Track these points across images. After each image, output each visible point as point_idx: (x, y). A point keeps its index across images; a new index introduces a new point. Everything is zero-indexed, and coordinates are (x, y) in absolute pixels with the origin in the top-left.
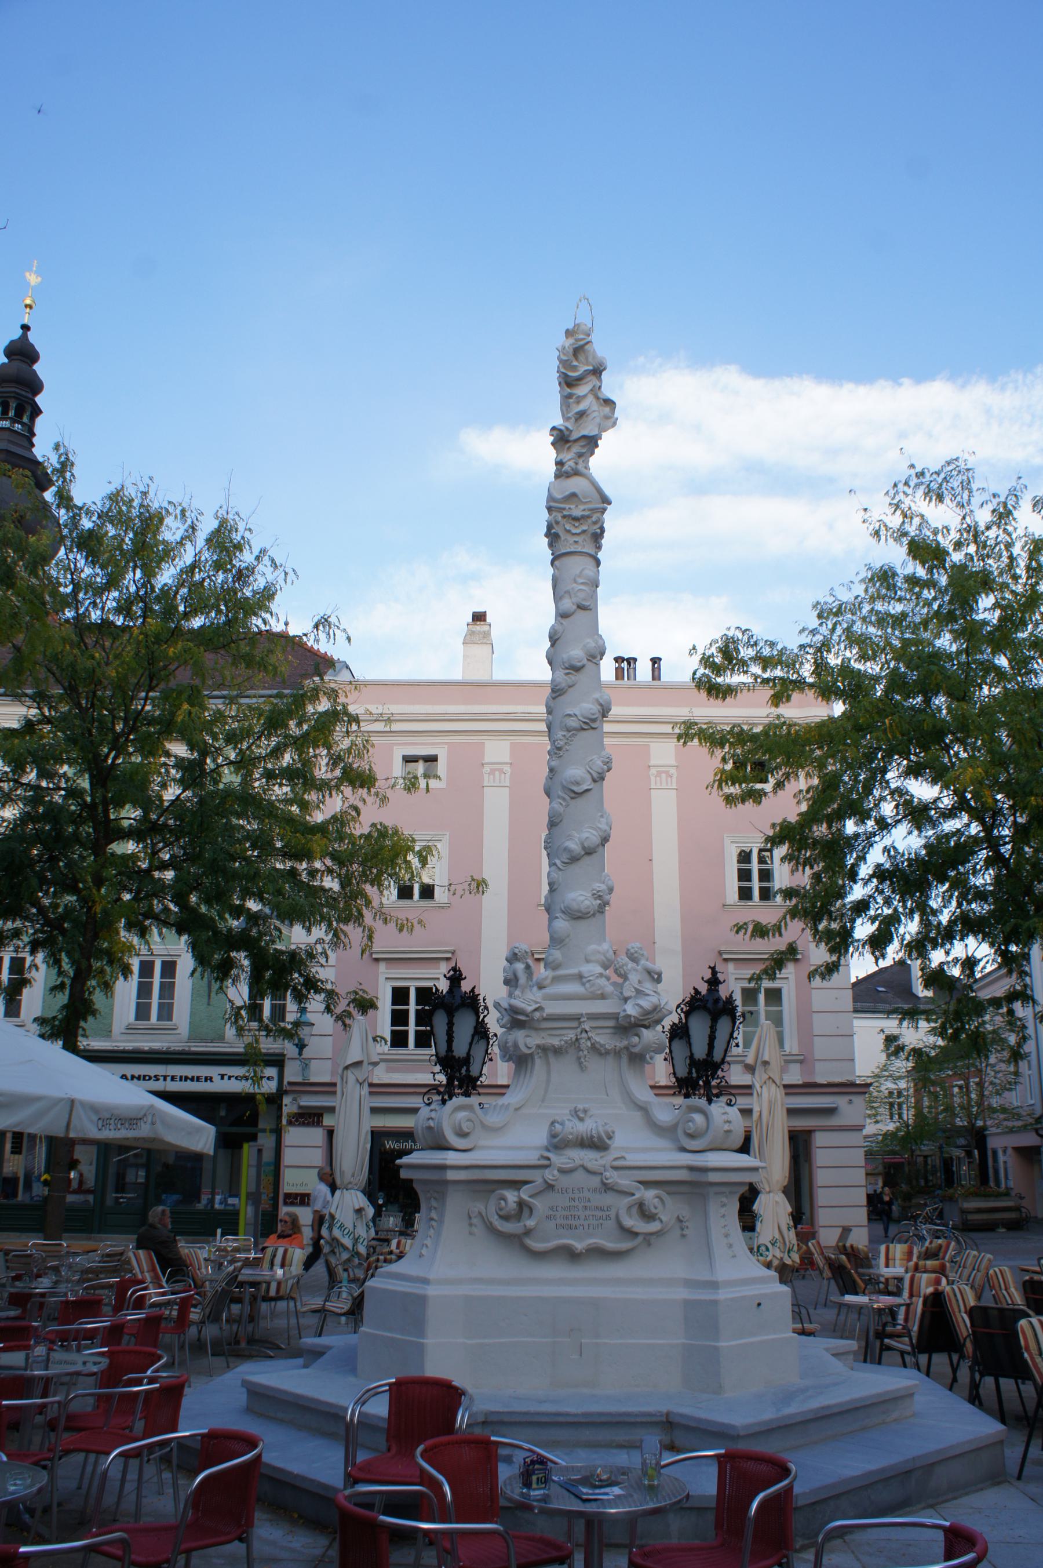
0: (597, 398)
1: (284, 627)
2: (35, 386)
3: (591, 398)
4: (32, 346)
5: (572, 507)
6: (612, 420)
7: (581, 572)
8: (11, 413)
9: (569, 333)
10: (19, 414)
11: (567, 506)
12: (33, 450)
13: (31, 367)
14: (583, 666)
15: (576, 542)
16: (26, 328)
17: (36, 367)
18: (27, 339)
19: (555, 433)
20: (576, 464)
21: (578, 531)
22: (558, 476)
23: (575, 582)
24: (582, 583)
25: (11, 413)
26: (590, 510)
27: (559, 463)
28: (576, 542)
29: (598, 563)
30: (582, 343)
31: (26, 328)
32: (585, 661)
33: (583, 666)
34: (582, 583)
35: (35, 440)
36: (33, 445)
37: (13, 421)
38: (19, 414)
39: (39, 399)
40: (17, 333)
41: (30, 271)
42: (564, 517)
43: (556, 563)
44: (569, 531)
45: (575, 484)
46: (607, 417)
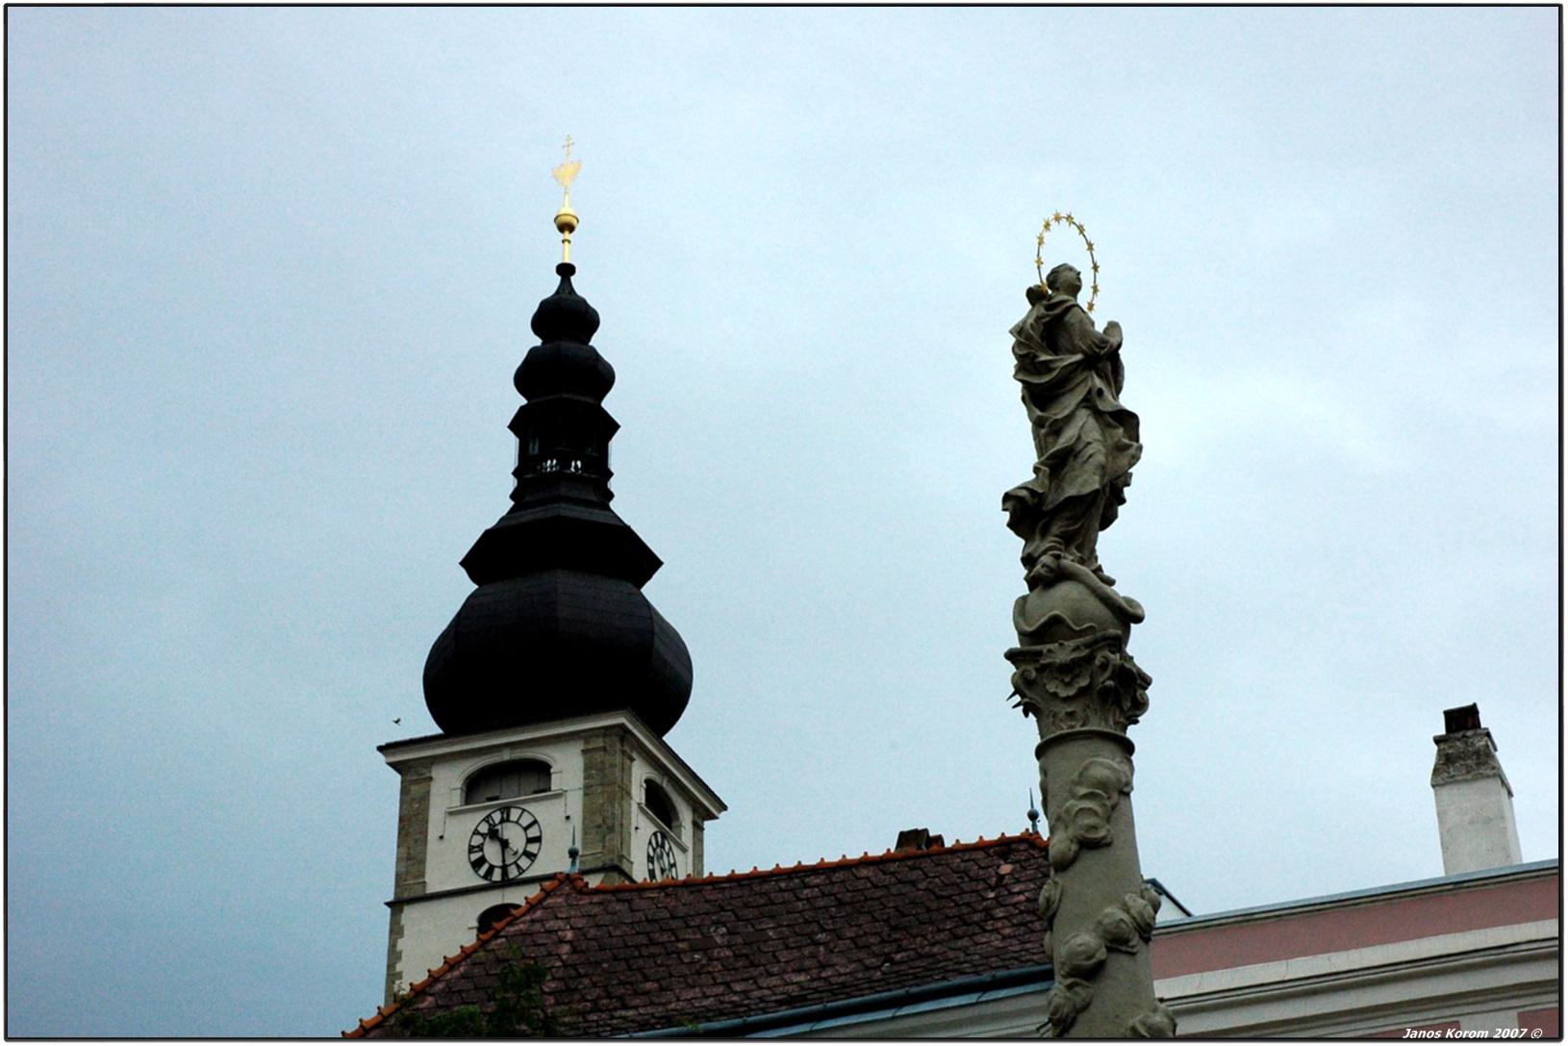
0: (1098, 414)
1: (1029, 824)
2: (602, 377)
3: (1083, 415)
4: (583, 302)
5: (1053, 646)
6: (1132, 451)
7: (1081, 775)
9: (1034, 295)
11: (1044, 648)
12: (613, 505)
13: (587, 344)
14: (1101, 965)
15: (1071, 715)
16: (566, 271)
17: (597, 341)
18: (572, 291)
19: (1009, 505)
20: (1058, 557)
21: (1072, 692)
22: (1033, 582)
23: (1073, 795)
24: (1085, 797)
26: (1087, 646)
27: (1028, 561)
28: (1071, 715)
29: (1128, 748)
30: (1058, 311)
31: (566, 271)
32: (1102, 954)
33: (1101, 965)
34: (1085, 797)
35: (613, 485)
36: (610, 496)
39: (610, 404)
40: (551, 284)
42: (1041, 670)
43: (1055, 754)
44: (1055, 695)
45: (1065, 598)
46: (1121, 448)
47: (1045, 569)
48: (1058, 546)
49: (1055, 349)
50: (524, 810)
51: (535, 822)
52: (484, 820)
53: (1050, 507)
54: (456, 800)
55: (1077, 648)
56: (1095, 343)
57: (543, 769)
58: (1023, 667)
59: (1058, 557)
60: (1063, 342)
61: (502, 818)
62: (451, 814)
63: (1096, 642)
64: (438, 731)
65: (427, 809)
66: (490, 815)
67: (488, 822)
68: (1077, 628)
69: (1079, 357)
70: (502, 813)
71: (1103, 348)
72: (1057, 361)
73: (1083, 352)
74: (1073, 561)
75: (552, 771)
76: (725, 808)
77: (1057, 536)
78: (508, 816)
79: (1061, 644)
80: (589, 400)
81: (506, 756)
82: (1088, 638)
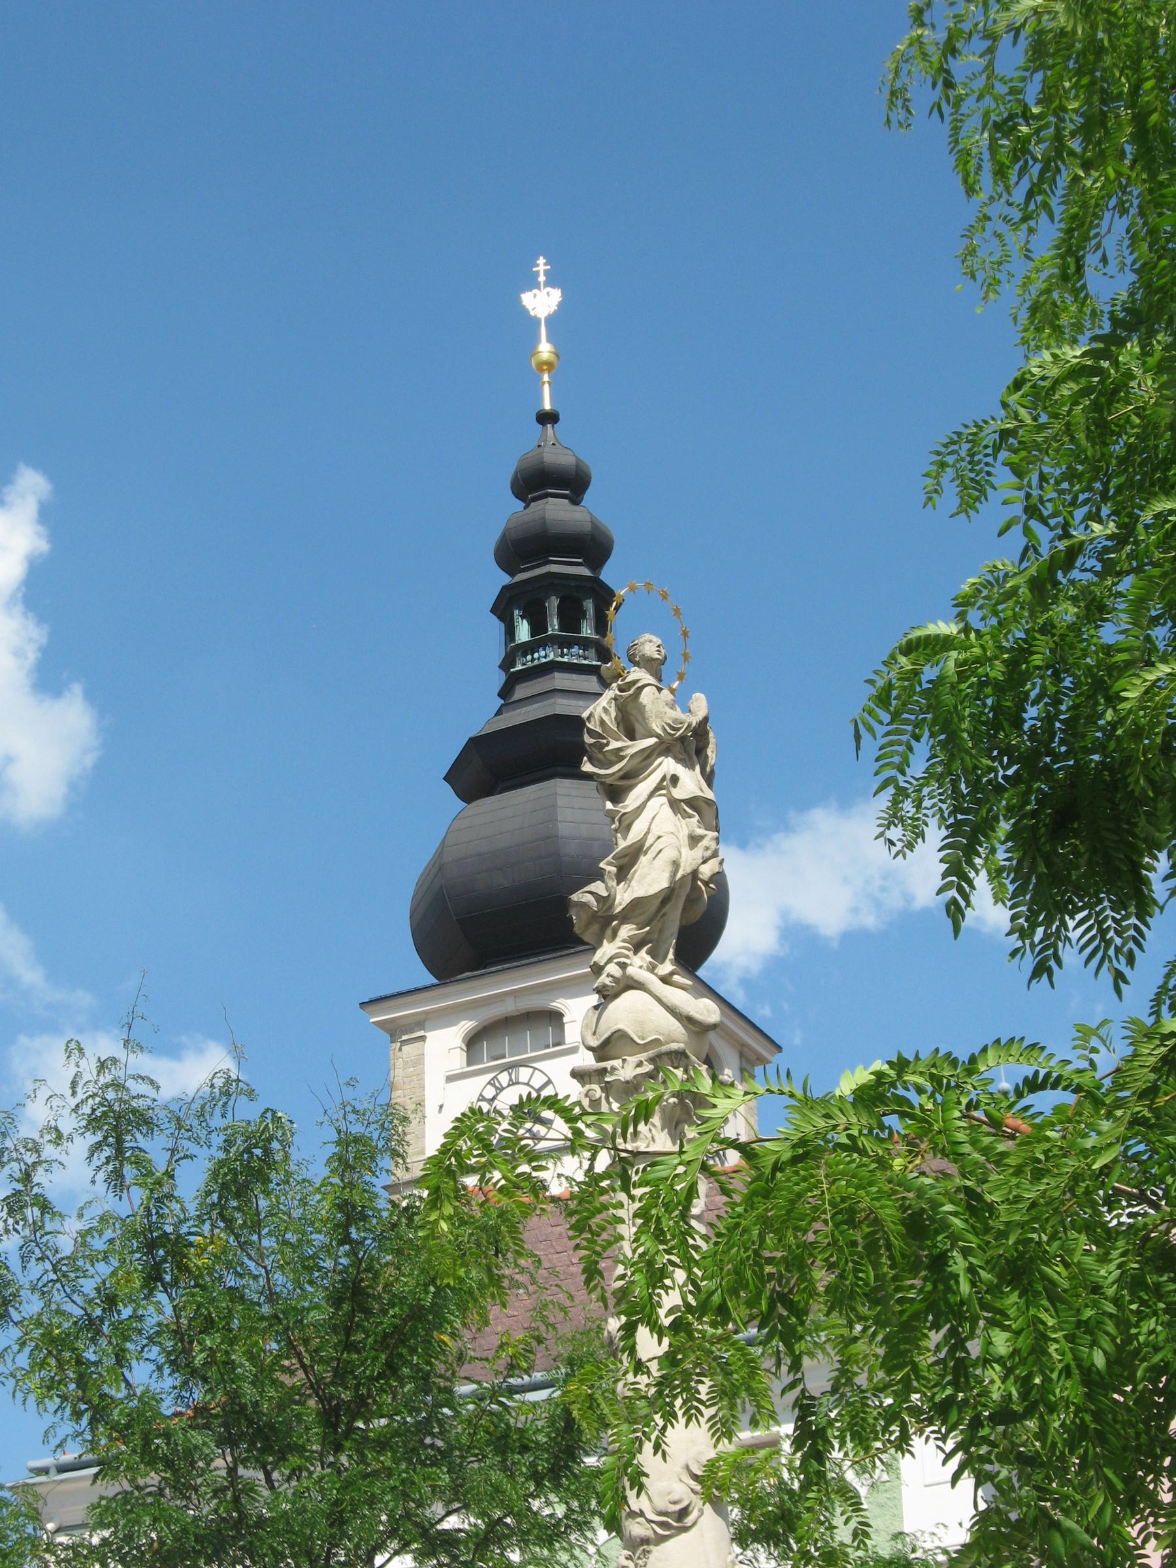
5: (617, 1063)
8: (554, 626)
10: (571, 620)
11: (608, 1064)
25: (554, 626)
37: (563, 643)
38: (571, 620)
41: (532, 284)
47: (610, 979)
48: (626, 952)
49: (632, 736)
50: (535, 1069)
51: (549, 1082)
52: (489, 1083)
53: (618, 910)
54: (457, 1060)
55: (640, 1064)
56: (669, 725)
57: (556, 1018)
58: (588, 1087)
59: (623, 966)
60: (639, 729)
61: (511, 1079)
62: (450, 1079)
63: (660, 1056)
64: (435, 981)
65: (420, 1075)
66: (495, 1077)
67: (494, 1085)
68: (641, 1042)
69: (652, 741)
70: (510, 1075)
71: (678, 729)
72: (628, 747)
73: (658, 736)
74: (641, 967)
75: (565, 1020)
76: (779, 1048)
77: (624, 941)
78: (517, 1076)
79: (624, 1061)
80: (585, 571)
81: (510, 1007)
82: (651, 1053)
